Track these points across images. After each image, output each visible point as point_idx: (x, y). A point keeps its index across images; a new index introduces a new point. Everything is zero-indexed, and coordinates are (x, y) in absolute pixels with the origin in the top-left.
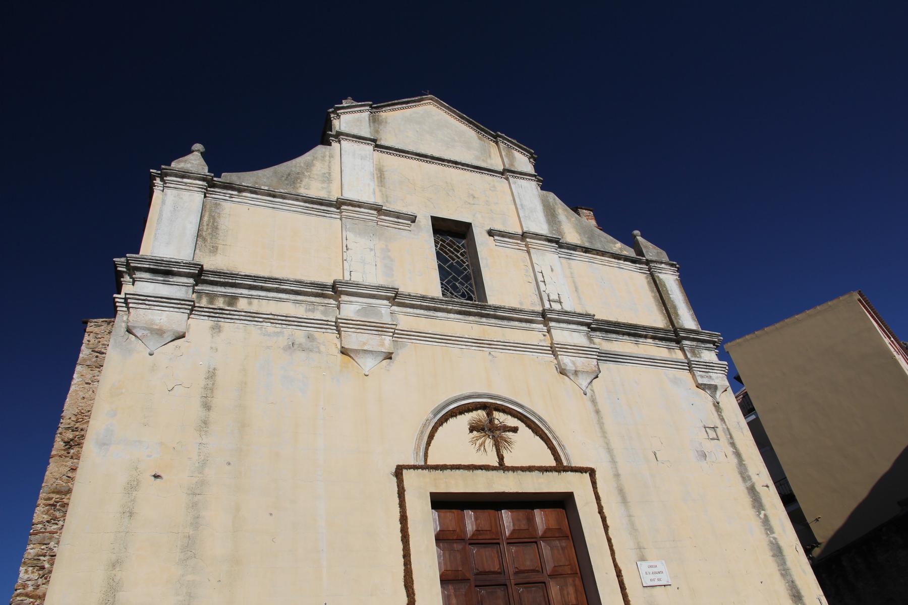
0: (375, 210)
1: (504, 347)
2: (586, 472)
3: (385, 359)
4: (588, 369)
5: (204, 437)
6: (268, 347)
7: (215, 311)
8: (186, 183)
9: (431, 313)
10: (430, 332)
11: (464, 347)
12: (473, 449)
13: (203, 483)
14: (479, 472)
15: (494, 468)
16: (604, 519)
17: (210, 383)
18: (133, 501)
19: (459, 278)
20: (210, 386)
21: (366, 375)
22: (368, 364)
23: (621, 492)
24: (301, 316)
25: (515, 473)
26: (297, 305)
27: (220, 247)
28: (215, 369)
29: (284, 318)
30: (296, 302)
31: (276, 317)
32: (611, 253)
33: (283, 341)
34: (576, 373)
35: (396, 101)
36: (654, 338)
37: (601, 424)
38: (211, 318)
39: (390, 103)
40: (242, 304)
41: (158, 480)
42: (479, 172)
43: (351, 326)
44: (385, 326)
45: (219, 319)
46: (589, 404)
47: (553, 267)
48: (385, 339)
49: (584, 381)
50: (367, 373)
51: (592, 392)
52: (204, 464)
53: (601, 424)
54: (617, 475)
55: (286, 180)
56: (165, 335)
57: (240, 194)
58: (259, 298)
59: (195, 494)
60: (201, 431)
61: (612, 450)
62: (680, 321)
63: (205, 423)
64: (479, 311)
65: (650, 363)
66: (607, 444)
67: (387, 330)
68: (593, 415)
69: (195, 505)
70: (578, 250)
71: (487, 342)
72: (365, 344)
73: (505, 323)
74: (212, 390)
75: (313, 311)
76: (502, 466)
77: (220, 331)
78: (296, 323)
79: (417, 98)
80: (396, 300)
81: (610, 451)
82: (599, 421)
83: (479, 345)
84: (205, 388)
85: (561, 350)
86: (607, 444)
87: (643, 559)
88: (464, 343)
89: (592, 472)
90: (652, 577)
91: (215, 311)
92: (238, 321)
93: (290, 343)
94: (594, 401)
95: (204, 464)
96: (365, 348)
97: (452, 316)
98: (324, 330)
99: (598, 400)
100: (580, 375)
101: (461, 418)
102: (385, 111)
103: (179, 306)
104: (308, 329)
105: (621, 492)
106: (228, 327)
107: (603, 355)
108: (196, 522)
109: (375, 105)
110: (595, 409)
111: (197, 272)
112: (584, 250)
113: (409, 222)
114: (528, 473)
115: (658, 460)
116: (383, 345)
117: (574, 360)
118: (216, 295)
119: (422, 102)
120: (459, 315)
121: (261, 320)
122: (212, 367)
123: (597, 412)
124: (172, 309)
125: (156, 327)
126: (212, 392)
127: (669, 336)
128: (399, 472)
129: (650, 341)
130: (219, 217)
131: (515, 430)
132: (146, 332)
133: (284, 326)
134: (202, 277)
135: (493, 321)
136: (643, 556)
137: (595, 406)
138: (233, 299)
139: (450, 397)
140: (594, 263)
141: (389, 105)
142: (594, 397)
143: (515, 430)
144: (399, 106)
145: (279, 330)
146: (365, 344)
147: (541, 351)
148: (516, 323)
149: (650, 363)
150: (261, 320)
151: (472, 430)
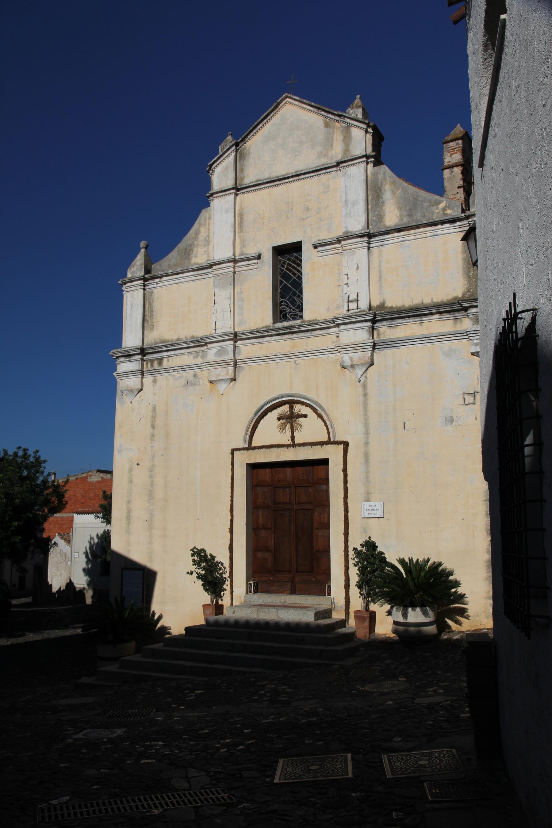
0: (231, 261)
1: (304, 356)
2: (341, 444)
3: (231, 381)
4: (363, 362)
5: (153, 443)
6: (176, 387)
7: (152, 371)
8: (134, 285)
9: (261, 340)
10: (256, 357)
11: (279, 361)
12: (277, 432)
13: (153, 466)
14: (274, 449)
15: (288, 446)
16: (346, 476)
17: (154, 414)
18: (131, 476)
19: (297, 292)
20: (154, 415)
21: (222, 395)
22: (223, 387)
23: (366, 456)
24: (189, 365)
25: (294, 448)
26: (189, 355)
27: (155, 324)
28: (155, 406)
29: (181, 368)
30: (189, 353)
31: (178, 368)
32: (424, 224)
33: (183, 382)
34: (353, 366)
35: (256, 123)
36: (440, 313)
37: (365, 405)
38: (152, 375)
39: (251, 128)
40: (165, 363)
41: (138, 466)
42: (318, 175)
43: (211, 365)
44: (228, 361)
45: (155, 375)
46: (360, 390)
47: (359, 265)
48: (229, 369)
49: (359, 371)
50: (222, 394)
51: (365, 379)
52: (153, 456)
53: (365, 405)
54: (367, 443)
55: (184, 254)
56: (134, 392)
57: (162, 280)
58: (172, 356)
59: (151, 471)
60: (151, 440)
61: (369, 424)
62: (466, 290)
63: (153, 436)
64: (289, 331)
65: (426, 342)
66: (366, 420)
67: (230, 363)
68: (361, 398)
69: (151, 476)
70: (391, 232)
71: (292, 355)
72: (219, 375)
73: (310, 334)
74: (155, 417)
75: (196, 357)
76: (293, 445)
77: (156, 383)
78: (188, 369)
79: (273, 107)
80: (238, 338)
81: (366, 425)
82: (364, 402)
83: (287, 358)
84: (152, 417)
85: (342, 350)
86: (366, 420)
87: (367, 500)
88: (278, 359)
89: (346, 444)
90: (370, 512)
91: (152, 371)
92: (163, 374)
93: (186, 382)
94: (365, 387)
95: (153, 456)
96: (219, 378)
97: (274, 338)
98: (202, 369)
99: (369, 385)
100: (356, 367)
101: (269, 415)
102: (259, 129)
103: (136, 374)
104: (194, 370)
105: (366, 456)
106: (159, 378)
107: (381, 344)
108: (152, 484)
109: (240, 139)
110: (364, 393)
111: (140, 352)
112: (397, 231)
113: (256, 261)
114: (302, 447)
115: (405, 428)
116: (228, 374)
117: (352, 356)
118: (154, 360)
119: (280, 107)
120: (278, 337)
121: (172, 371)
122: (154, 405)
123: (365, 395)
124: (134, 377)
125: (130, 389)
126: (155, 419)
127: (453, 309)
128: (233, 451)
129: (437, 316)
130: (153, 302)
131: (305, 416)
132: (127, 392)
133: (183, 371)
134: (145, 352)
135: (301, 334)
136: (369, 498)
137: (364, 390)
138: (160, 360)
139: (266, 400)
140: (405, 241)
141: (252, 131)
142: (366, 383)
143: (305, 416)
144: (260, 125)
145: (180, 375)
146: (219, 375)
147: (330, 353)
148: (318, 332)
149: (426, 342)
150: (172, 371)
151: (279, 419)
